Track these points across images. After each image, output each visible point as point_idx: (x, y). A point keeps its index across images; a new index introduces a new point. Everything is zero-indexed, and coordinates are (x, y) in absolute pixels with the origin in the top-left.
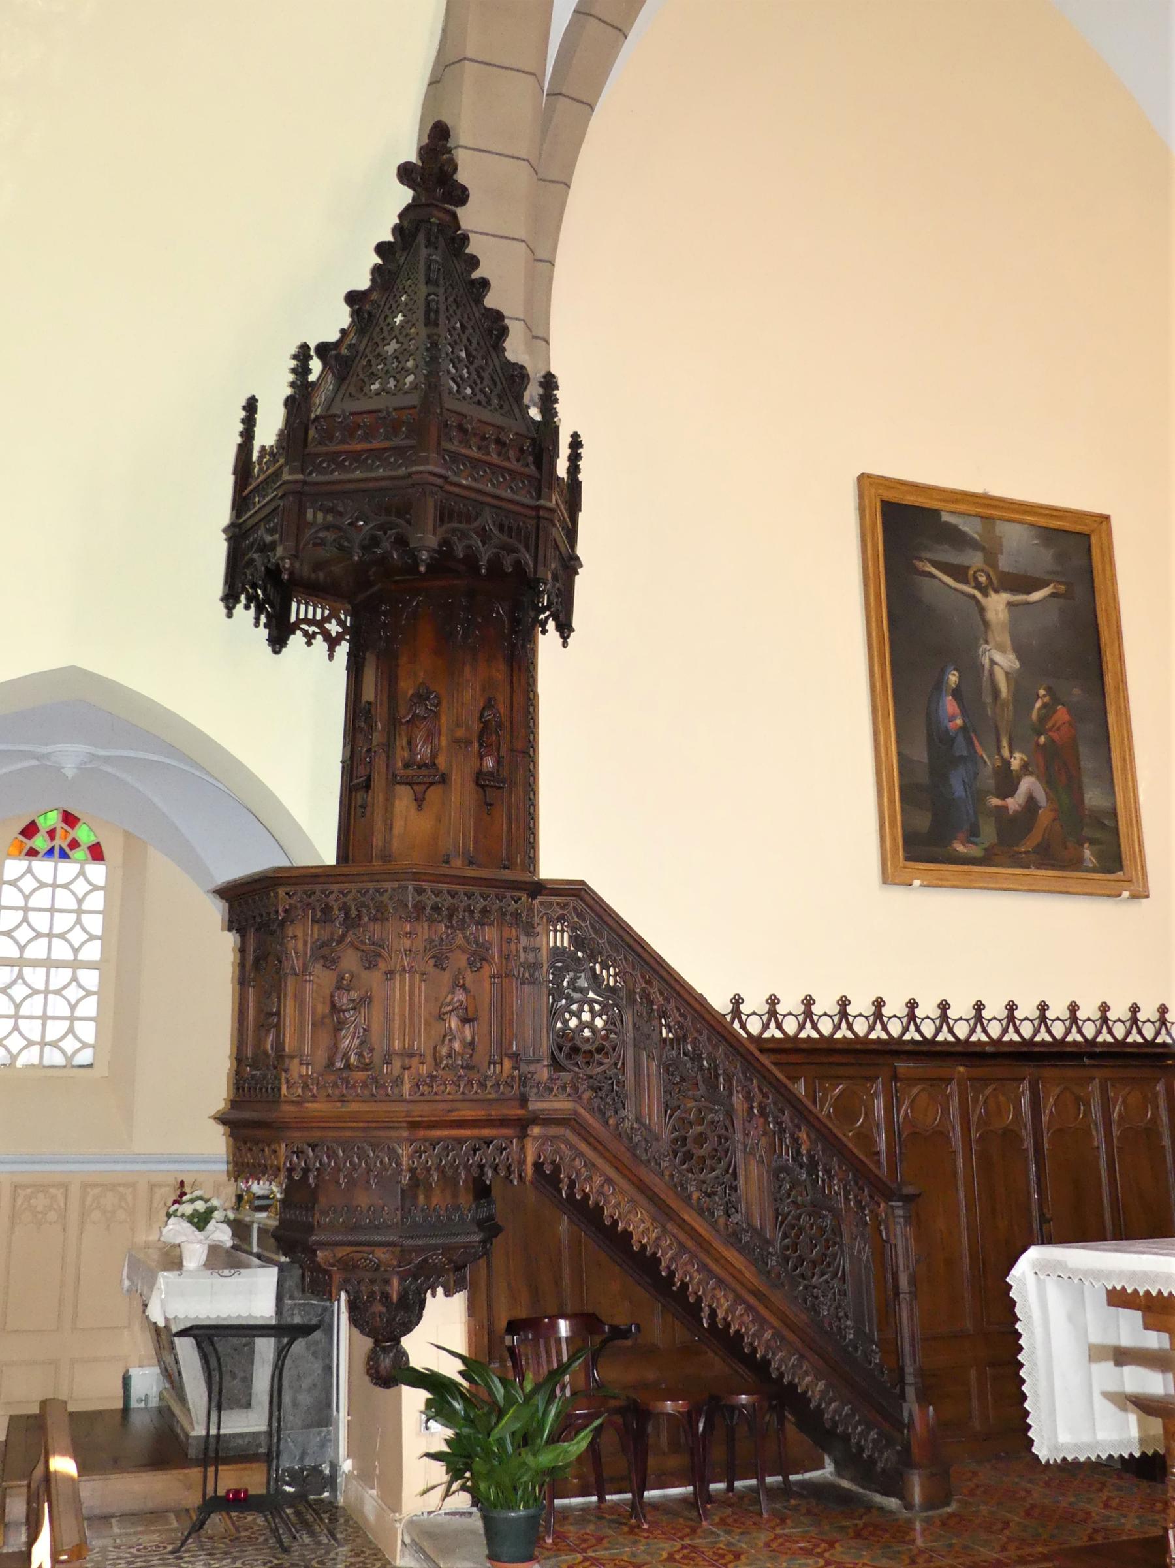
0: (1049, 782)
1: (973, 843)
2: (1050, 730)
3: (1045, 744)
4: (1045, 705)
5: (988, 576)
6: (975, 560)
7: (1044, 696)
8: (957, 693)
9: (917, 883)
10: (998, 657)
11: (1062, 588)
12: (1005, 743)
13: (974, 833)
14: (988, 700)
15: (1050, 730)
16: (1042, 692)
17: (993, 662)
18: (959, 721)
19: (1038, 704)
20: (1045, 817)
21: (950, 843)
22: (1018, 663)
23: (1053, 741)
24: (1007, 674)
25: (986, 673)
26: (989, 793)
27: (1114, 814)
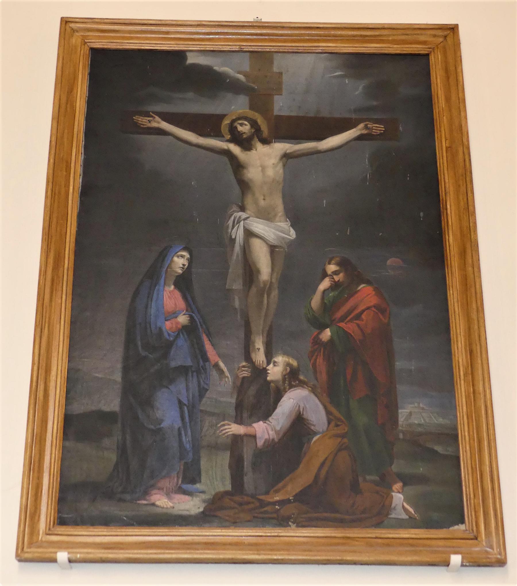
0: (333, 393)
1: (185, 492)
2: (342, 319)
3: (331, 341)
4: (335, 286)
5: (254, 124)
6: (236, 106)
7: (336, 273)
8: (183, 283)
9: (456, 559)
10: (259, 226)
11: (378, 128)
12: (259, 344)
13: (191, 476)
14: (236, 285)
15: (342, 319)
16: (332, 268)
17: (249, 234)
18: (183, 319)
19: (325, 284)
20: (321, 448)
21: (146, 493)
22: (293, 232)
23: (347, 335)
24: (273, 249)
25: (237, 248)
26: (224, 417)
27: (451, 436)
